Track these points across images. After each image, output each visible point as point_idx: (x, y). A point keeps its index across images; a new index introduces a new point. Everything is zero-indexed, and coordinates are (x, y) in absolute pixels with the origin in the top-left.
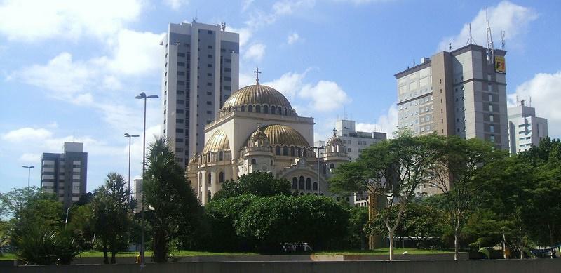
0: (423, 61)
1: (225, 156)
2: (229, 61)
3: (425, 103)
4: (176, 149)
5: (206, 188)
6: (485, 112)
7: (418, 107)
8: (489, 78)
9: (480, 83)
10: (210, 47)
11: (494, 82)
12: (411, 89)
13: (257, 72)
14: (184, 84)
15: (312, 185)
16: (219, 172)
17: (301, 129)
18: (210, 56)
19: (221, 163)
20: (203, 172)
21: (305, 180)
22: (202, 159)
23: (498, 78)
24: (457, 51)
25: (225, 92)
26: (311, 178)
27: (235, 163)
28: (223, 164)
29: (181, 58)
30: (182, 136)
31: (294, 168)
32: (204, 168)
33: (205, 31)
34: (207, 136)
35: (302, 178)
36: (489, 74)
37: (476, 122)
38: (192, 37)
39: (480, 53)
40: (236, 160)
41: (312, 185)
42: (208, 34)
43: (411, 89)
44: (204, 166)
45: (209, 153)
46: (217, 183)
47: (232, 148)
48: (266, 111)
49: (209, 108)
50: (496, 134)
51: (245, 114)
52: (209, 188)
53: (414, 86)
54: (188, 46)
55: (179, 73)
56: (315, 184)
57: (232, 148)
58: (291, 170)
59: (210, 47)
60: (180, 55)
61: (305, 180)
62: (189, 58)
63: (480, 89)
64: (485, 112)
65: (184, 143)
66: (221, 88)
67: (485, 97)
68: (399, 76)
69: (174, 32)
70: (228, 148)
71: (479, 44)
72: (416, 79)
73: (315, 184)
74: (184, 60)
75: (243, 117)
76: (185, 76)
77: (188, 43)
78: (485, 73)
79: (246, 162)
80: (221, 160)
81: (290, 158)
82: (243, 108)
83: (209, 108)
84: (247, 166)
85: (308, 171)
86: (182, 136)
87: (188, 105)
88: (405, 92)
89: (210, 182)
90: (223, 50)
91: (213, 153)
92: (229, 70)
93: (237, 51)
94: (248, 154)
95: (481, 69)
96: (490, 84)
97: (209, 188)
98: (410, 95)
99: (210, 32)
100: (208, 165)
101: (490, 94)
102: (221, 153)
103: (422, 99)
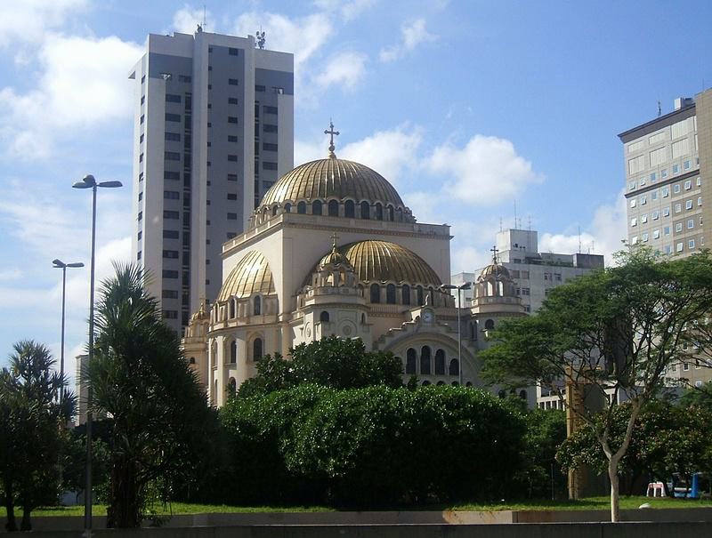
0: (678, 105)
1: (267, 306)
2: (273, 110)
3: (683, 192)
5: (226, 373)
7: (669, 200)
10: (233, 82)
12: (654, 164)
13: (332, 133)
15: (448, 363)
16: (252, 342)
17: (424, 249)
18: (233, 120)
19: (258, 320)
20: (220, 340)
21: (433, 354)
22: (218, 313)
25: (264, 174)
26: (444, 348)
27: (286, 321)
28: (234, 325)
30: (177, 265)
31: (410, 330)
32: (221, 332)
34: (228, 265)
35: (426, 350)
38: (196, 67)
40: (289, 313)
41: (448, 363)
42: (228, 55)
43: (654, 164)
44: (221, 326)
45: (232, 300)
46: (248, 362)
47: (279, 290)
48: (350, 212)
51: (306, 219)
52: (232, 373)
53: (659, 158)
54: (188, 79)
55: (170, 136)
56: (455, 362)
57: (279, 290)
58: (403, 334)
59: (233, 82)
60: (170, 98)
61: (433, 354)
62: (189, 105)
65: (180, 240)
66: (257, 183)
68: (627, 136)
70: (271, 288)
72: (663, 142)
73: (455, 362)
74: (179, 109)
75: (303, 226)
76: (183, 104)
77: (188, 75)
79: (310, 317)
80: (257, 313)
81: (400, 308)
82: (302, 207)
84: (311, 326)
85: (437, 335)
87: (187, 201)
88: (642, 168)
89: (234, 360)
90: (259, 88)
91: (240, 300)
92: (272, 129)
93: (289, 91)
94: (313, 302)
97: (232, 373)
98: (653, 177)
99: (234, 52)
100: (231, 325)
102: (257, 299)
103: (678, 185)
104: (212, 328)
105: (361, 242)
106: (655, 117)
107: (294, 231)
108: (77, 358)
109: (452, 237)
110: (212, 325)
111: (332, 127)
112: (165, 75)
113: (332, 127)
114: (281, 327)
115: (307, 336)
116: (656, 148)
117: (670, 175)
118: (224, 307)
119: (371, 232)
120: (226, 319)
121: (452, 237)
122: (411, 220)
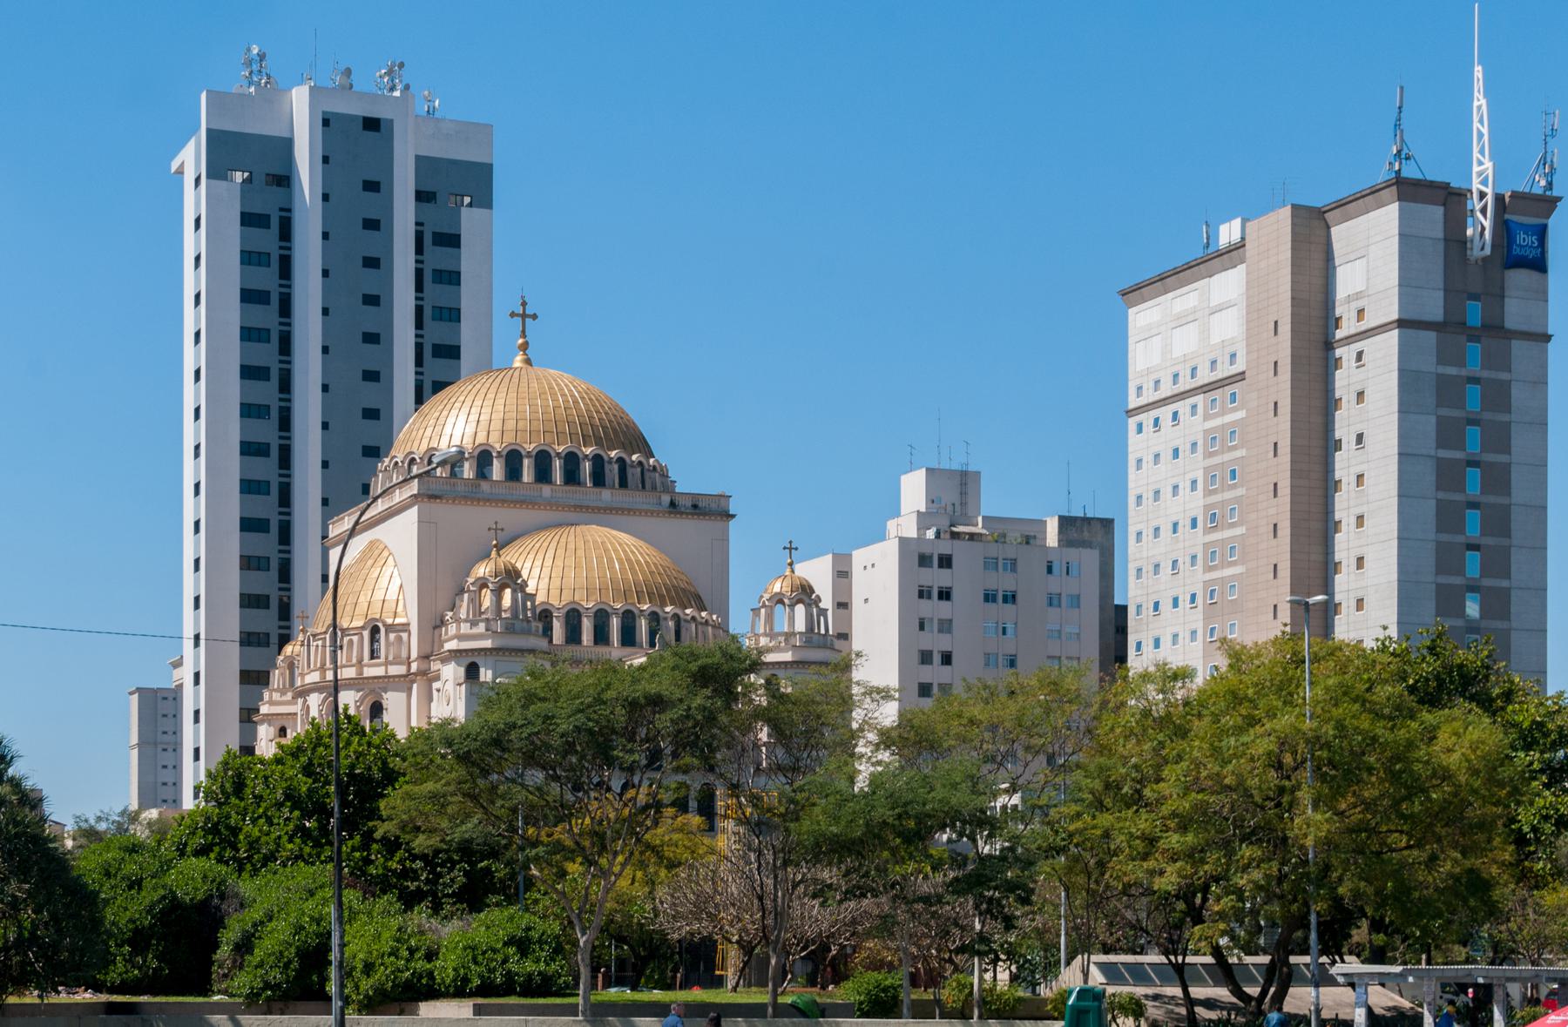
4: (240, 747)
6: (1443, 454)
8: (1474, 313)
9: (1430, 337)
10: (372, 186)
11: (1495, 329)
13: (524, 316)
14: (268, 302)
23: (1515, 314)
24: (1341, 204)
25: (435, 367)
28: (380, 671)
29: (254, 574)
30: (267, 392)
33: (323, 474)
36: (1474, 297)
37: (1400, 496)
39: (1439, 211)
49: (369, 395)
50: (1489, 541)
53: (1185, 343)
54: (284, 180)
63: (1428, 363)
64: (1443, 454)
67: (1448, 391)
69: (247, 210)
71: (1431, 176)
76: (274, 573)
78: (1454, 293)
83: (369, 395)
86: (266, 507)
90: (423, 196)
93: (484, 199)
95: (1438, 278)
96: (1474, 338)
100: (369, 672)
101: (1474, 380)
103: (1217, 394)
104: (303, 679)
105: (568, 525)
106: (1199, 253)
107: (438, 508)
108: (268, 175)
109: (733, 516)
110: (303, 675)
111: (524, 304)
112: (239, 174)
113: (524, 304)
114: (413, 682)
115: (445, 704)
116: (1182, 321)
117: (1205, 376)
118: (320, 643)
119: (579, 508)
120: (360, 661)
121: (733, 516)
122: (668, 486)
